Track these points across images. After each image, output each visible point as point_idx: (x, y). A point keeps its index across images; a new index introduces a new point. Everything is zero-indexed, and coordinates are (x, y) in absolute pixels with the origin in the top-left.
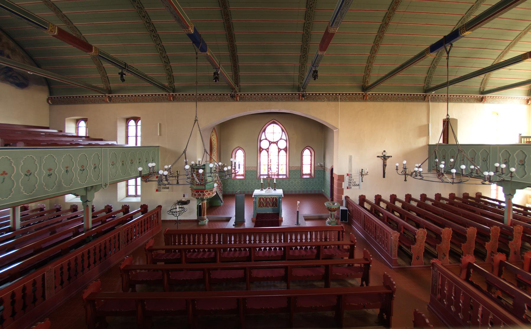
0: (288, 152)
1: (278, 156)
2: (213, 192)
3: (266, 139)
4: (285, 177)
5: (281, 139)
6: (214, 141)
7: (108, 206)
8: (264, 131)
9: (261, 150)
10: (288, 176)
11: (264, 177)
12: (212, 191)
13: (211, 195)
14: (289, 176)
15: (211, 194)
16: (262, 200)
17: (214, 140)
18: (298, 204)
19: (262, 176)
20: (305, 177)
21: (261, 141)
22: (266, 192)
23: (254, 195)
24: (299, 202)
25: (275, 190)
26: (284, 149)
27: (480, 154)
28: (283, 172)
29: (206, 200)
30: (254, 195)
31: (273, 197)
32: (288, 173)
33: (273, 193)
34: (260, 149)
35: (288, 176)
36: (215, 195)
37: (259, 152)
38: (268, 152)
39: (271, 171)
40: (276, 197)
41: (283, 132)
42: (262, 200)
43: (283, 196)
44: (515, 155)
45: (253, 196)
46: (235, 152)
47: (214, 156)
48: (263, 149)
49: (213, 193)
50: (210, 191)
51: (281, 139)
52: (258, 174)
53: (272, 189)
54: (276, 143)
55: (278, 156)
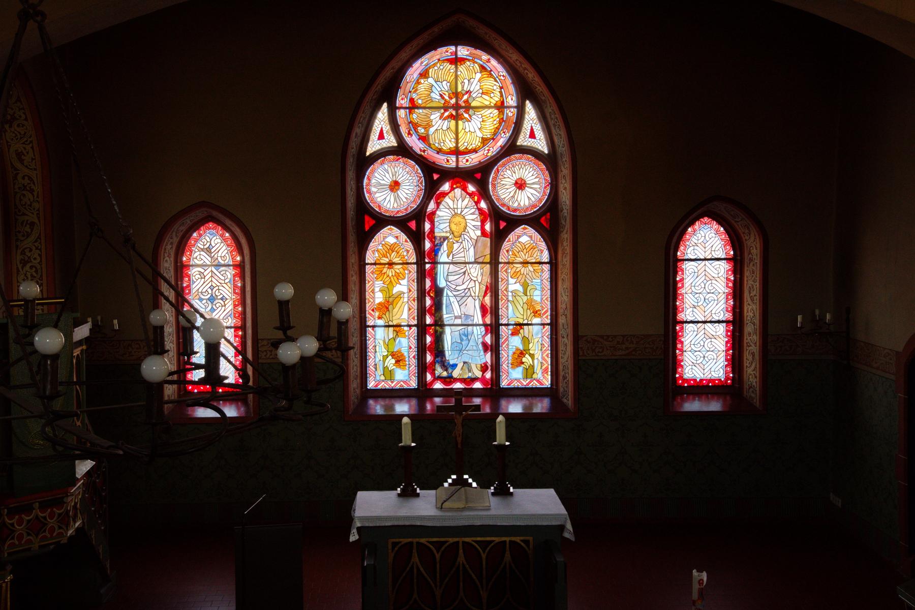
0: (566, 237)
1: (494, 262)
2: (67, 512)
3: (402, 151)
4: (541, 406)
5: (511, 149)
6: (18, 165)
7: (397, 496)
8: (389, 94)
9: (369, 222)
10: (569, 401)
11: (392, 408)
12: (60, 502)
13: (52, 530)
14: (576, 399)
15: (52, 522)
16: (415, 559)
17: (19, 155)
18: (696, 587)
19: (382, 402)
20: (693, 406)
21: (365, 162)
22: (446, 505)
23: (359, 529)
24: (704, 576)
25: (502, 492)
26: (532, 220)
27: (10, 520)
28: (529, 372)
29: (9, 567)
30: (359, 529)
31: (451, 540)
32: (570, 377)
33: (493, 512)
34: (360, 223)
35: (569, 401)
36: (78, 530)
37: (352, 238)
38: (417, 238)
39: (445, 366)
40: (517, 539)
41: (529, 106)
42: (415, 559)
43: (569, 533)
44: (18, 527)
45: (354, 537)
46: (176, 240)
47: (24, 263)
48: (382, 221)
49: (65, 521)
50: (43, 507)
51: (511, 149)
52: (354, 385)
53: (484, 485)
54: (478, 176)
55: (494, 262)
